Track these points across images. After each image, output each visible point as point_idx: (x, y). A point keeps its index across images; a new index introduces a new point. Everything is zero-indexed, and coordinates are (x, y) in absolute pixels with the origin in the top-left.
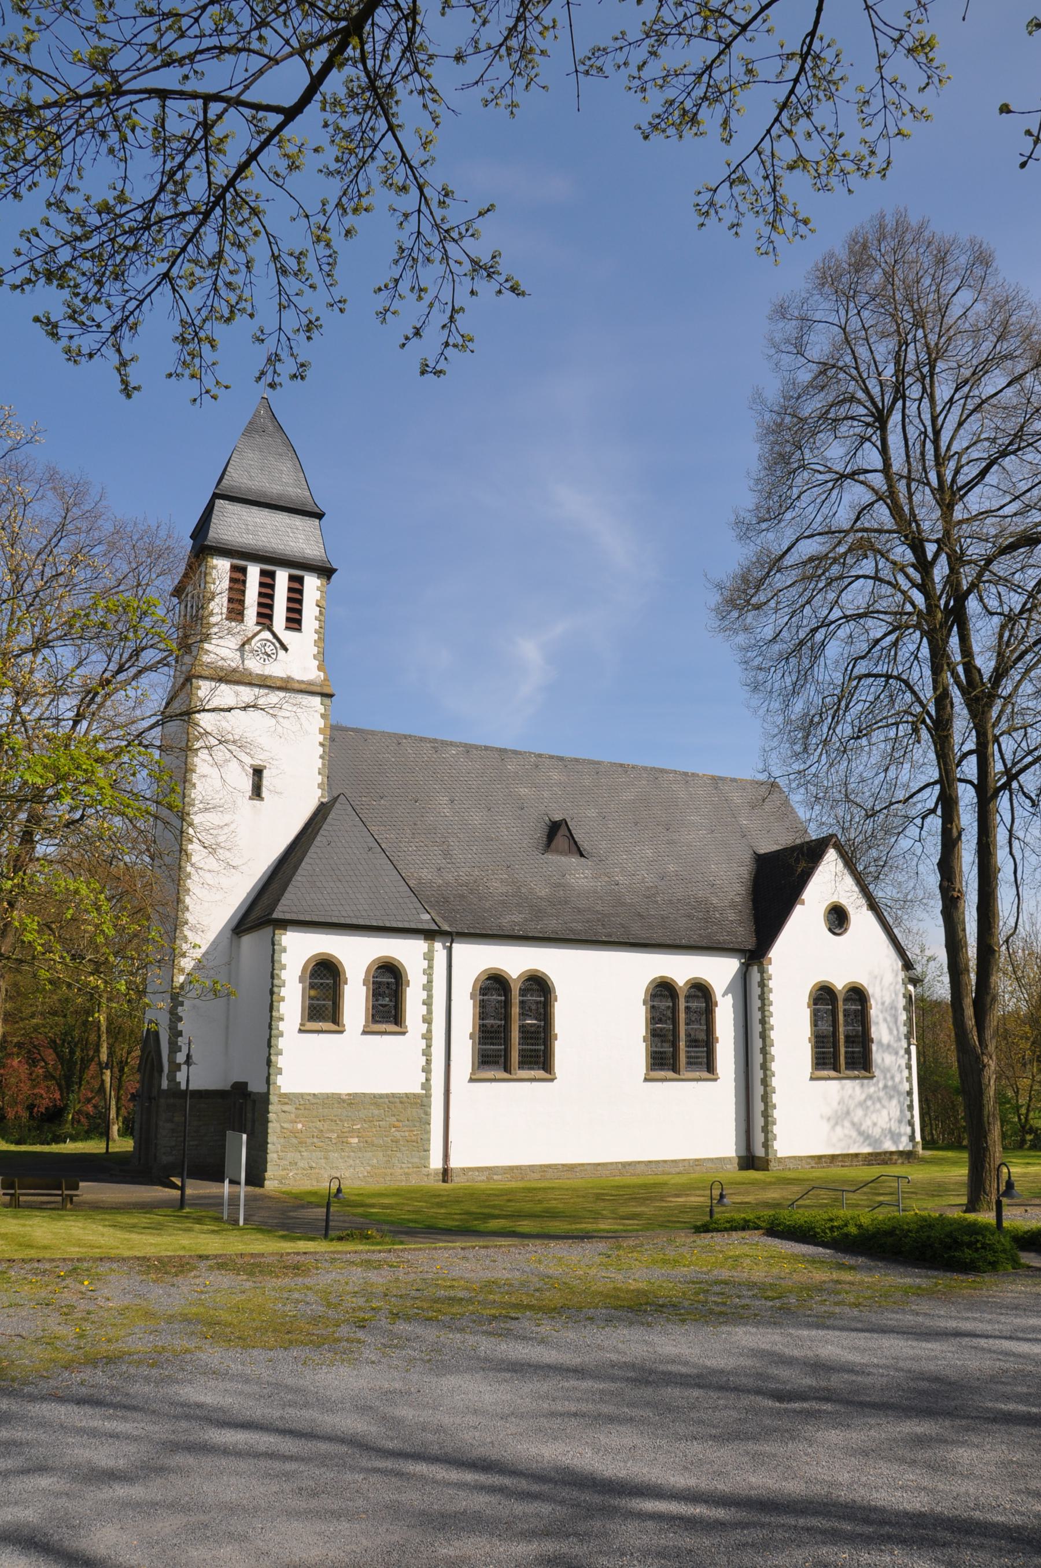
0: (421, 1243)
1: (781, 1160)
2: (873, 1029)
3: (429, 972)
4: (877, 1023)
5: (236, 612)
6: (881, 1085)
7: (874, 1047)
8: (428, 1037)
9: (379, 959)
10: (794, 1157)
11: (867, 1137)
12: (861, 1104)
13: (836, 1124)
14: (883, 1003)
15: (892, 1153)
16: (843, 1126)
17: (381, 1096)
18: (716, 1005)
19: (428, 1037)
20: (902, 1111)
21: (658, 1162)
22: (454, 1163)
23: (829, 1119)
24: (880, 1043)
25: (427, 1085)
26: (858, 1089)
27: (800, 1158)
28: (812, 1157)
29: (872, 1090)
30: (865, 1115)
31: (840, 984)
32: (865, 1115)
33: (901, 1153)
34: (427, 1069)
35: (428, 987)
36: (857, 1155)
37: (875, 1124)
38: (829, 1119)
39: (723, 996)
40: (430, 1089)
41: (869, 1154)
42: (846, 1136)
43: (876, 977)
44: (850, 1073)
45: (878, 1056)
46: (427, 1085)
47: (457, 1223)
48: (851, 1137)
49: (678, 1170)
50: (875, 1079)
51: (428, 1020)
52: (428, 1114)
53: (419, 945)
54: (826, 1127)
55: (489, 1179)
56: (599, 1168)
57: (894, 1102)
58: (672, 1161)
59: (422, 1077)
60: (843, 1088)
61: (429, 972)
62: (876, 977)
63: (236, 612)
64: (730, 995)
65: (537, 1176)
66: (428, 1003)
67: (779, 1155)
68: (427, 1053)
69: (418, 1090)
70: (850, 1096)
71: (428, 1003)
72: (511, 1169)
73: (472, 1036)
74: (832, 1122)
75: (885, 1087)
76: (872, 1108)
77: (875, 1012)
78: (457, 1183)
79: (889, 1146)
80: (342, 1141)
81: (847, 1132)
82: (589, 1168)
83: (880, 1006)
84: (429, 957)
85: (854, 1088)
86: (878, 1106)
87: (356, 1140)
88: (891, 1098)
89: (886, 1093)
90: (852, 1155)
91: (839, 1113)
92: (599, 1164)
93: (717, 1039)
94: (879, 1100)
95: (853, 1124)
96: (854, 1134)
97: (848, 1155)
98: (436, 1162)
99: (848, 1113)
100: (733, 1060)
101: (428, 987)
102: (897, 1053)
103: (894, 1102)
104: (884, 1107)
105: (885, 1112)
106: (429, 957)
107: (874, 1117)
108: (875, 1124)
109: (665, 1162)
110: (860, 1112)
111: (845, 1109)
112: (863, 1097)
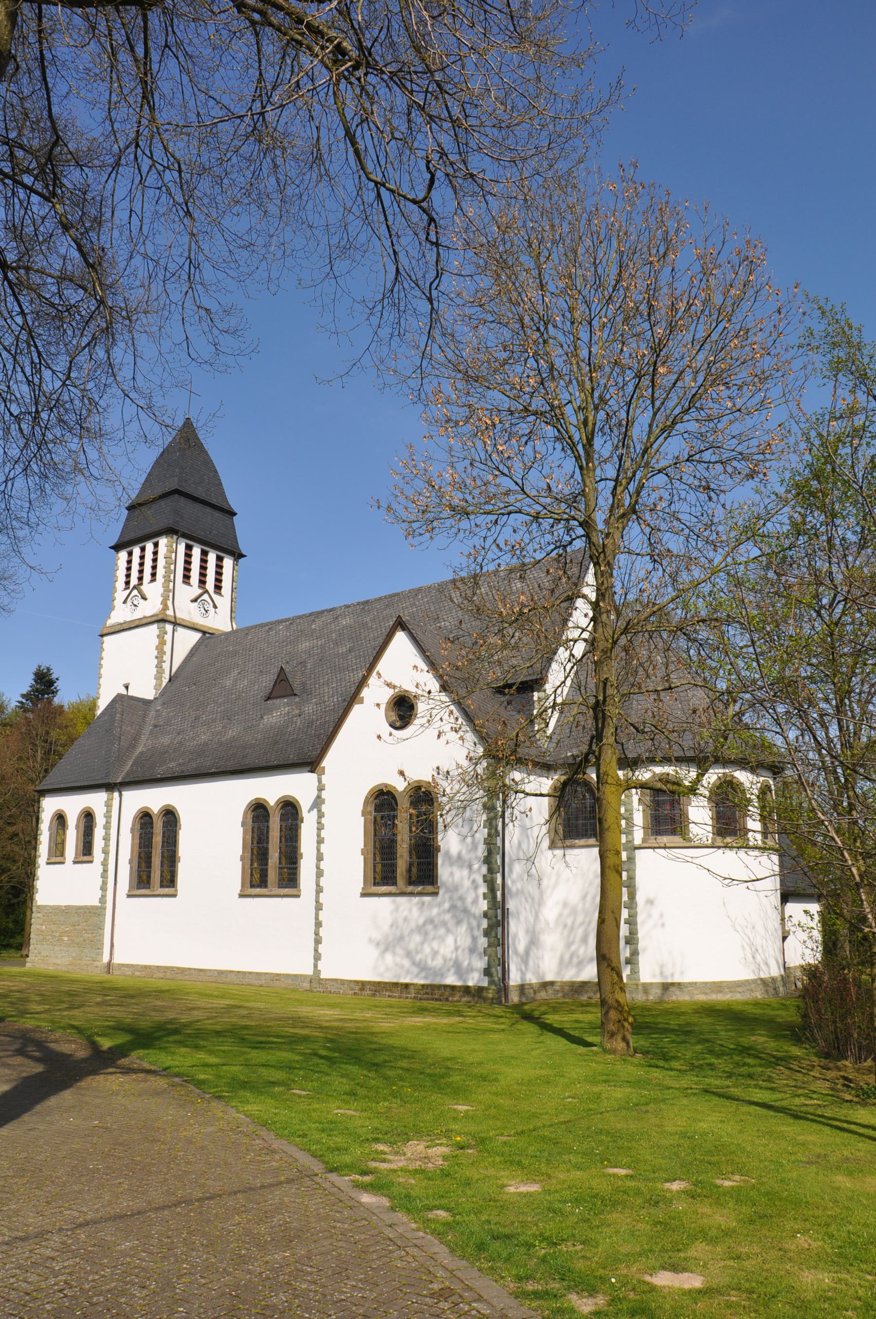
0: (282, 1031)
5: (187, 578)
6: (447, 905)
8: (105, 864)
9: (174, 807)
10: (336, 980)
11: (423, 967)
12: (420, 929)
13: (386, 949)
15: (453, 988)
16: (394, 953)
17: (80, 908)
18: (302, 821)
20: (474, 939)
21: (244, 973)
22: (117, 960)
23: (378, 944)
24: (447, 854)
25: (103, 899)
26: (415, 912)
27: (343, 982)
28: (357, 982)
29: (435, 911)
30: (422, 943)
33: (466, 990)
35: (107, 827)
36: (407, 986)
38: (378, 944)
39: (309, 812)
40: (105, 903)
41: (423, 986)
42: (396, 964)
44: (410, 889)
45: (444, 872)
46: (103, 899)
48: (402, 967)
49: (260, 983)
50: (439, 898)
51: (106, 852)
54: (374, 953)
56: (202, 973)
57: (463, 928)
58: (257, 973)
60: (397, 909)
63: (187, 578)
65: (160, 975)
66: (106, 838)
67: (322, 977)
71: (106, 838)
72: (146, 967)
74: (382, 947)
75: (453, 907)
79: (451, 980)
80: (60, 939)
81: (398, 960)
82: (193, 972)
85: (410, 910)
87: (66, 938)
88: (459, 922)
89: (454, 916)
90: (402, 984)
91: (390, 938)
92: (201, 970)
93: (301, 855)
94: (444, 924)
95: (408, 954)
96: (406, 963)
97: (396, 984)
98: (106, 959)
101: (107, 827)
102: (470, 867)
103: (463, 928)
104: (448, 931)
105: (450, 940)
106: (108, 805)
107: (435, 945)
108: (435, 953)
109: (250, 973)
110: (417, 938)
111: (398, 934)
112: (421, 921)
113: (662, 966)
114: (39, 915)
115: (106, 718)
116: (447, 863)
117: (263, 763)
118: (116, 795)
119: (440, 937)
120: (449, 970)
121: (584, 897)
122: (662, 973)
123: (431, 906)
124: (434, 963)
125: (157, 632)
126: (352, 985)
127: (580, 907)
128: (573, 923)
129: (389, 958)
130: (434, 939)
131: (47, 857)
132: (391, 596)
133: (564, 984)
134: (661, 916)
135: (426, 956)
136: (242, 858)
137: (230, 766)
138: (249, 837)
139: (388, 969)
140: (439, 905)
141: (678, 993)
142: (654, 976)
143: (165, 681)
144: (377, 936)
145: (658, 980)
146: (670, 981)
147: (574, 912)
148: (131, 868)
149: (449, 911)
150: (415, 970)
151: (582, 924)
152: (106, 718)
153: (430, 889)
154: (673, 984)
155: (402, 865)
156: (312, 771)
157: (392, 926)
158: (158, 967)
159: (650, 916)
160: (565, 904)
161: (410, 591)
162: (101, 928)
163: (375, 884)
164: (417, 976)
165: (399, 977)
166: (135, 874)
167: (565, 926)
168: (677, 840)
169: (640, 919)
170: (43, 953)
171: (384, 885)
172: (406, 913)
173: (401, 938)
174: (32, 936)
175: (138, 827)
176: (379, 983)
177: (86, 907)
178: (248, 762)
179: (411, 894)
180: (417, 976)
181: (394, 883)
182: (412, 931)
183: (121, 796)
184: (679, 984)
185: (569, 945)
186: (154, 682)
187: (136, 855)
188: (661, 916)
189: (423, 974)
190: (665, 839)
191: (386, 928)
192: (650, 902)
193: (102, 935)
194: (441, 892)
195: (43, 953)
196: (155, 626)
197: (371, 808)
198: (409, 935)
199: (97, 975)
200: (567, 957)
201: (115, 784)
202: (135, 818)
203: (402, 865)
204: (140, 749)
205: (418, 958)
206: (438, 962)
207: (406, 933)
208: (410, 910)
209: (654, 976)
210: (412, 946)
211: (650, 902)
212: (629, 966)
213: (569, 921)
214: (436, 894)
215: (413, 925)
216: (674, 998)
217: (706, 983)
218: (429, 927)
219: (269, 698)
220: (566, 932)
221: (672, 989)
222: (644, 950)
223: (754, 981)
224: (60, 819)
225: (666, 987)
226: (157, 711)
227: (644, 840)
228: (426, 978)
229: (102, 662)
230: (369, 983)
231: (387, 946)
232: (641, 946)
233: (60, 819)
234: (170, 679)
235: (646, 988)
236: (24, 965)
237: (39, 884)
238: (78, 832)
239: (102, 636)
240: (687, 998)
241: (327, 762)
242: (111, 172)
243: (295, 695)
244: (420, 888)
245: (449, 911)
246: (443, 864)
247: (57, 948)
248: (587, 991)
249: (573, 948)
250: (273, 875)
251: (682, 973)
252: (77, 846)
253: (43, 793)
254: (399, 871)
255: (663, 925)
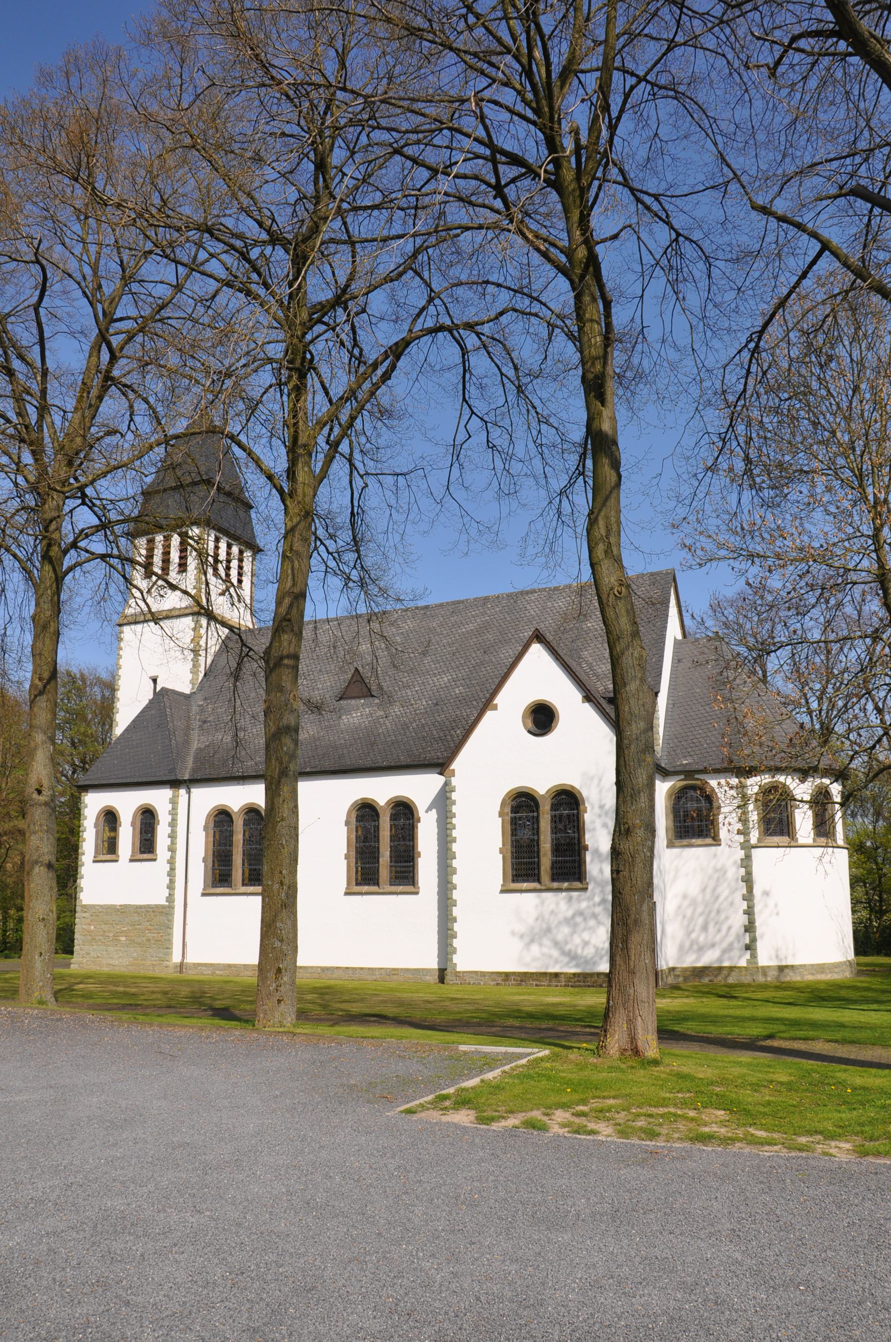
1: (457, 974)
2: (587, 836)
3: (174, 813)
4: (594, 829)
6: (597, 899)
7: (588, 857)
8: (172, 862)
11: (573, 957)
12: (568, 921)
13: (532, 941)
14: (602, 807)
16: (541, 945)
17: (141, 907)
19: (172, 862)
23: (522, 936)
25: (170, 898)
26: (563, 906)
27: (483, 974)
28: (499, 974)
29: (584, 905)
30: (572, 934)
31: (542, 786)
32: (572, 934)
34: (171, 886)
35: (173, 824)
36: (556, 975)
37: (586, 943)
38: (522, 936)
39: (427, 811)
41: (574, 974)
42: (544, 955)
43: (592, 778)
44: (555, 885)
46: (170, 898)
47: (673, 1051)
48: (550, 957)
49: (374, 977)
50: (588, 893)
51: (172, 849)
52: (171, 921)
53: (166, 793)
55: (213, 974)
59: (166, 892)
60: (543, 903)
61: (174, 813)
62: (592, 778)
64: (434, 811)
66: (173, 836)
67: (458, 969)
68: (172, 873)
69: (163, 902)
70: (552, 912)
71: (173, 836)
72: (229, 966)
73: (419, 855)
74: (527, 939)
76: (582, 925)
77: (588, 818)
78: (190, 975)
80: (116, 938)
81: (545, 950)
83: (597, 810)
84: (174, 802)
85: (557, 904)
86: (592, 923)
87: (123, 939)
90: (551, 974)
91: (536, 930)
93: (419, 854)
94: (594, 916)
95: (556, 944)
96: (555, 953)
97: (545, 974)
99: (548, 930)
100: (436, 874)
101: (173, 824)
106: (174, 802)
107: (586, 936)
109: (362, 969)
110: (566, 930)
111: (544, 926)
112: (570, 913)
113: (777, 951)
114: (85, 915)
115: (153, 712)
116: (596, 860)
117: (369, 764)
118: (182, 792)
119: (590, 928)
120: (601, 958)
121: (704, 890)
122: (777, 956)
123: (579, 901)
124: (585, 953)
125: (192, 625)
126: (493, 977)
127: (700, 898)
128: (693, 913)
129: (535, 949)
130: (584, 930)
131: (93, 854)
132: (453, 603)
133: (685, 970)
134: (776, 906)
135: (577, 946)
136: (347, 857)
137: (327, 765)
138: (353, 836)
139: (535, 959)
140: (589, 899)
141: (791, 974)
142: (771, 959)
143: (201, 675)
144: (521, 928)
145: (774, 963)
146: (784, 963)
147: (694, 903)
148: (206, 866)
149: (599, 904)
150: (566, 959)
151: (701, 914)
152: (153, 712)
153: (577, 884)
154: (787, 967)
155: (546, 861)
156: (441, 774)
157: (537, 919)
158: (245, 965)
159: (766, 906)
160: (685, 897)
161: (475, 599)
162: (169, 927)
163: (357, 884)
164: (567, 964)
165: (547, 967)
166: (210, 872)
167: (684, 917)
168: (785, 839)
169: (757, 909)
170: (93, 954)
171: (366, 884)
172: (552, 907)
173: (548, 930)
174: (76, 936)
175: (212, 825)
176: (525, 973)
177: (149, 906)
178: (348, 762)
179: (559, 890)
180: (567, 964)
181: (377, 884)
182: (560, 923)
183: (189, 793)
184: (792, 966)
185: (689, 934)
186: (190, 676)
187: (211, 853)
188: (776, 906)
189: (574, 963)
190: (776, 839)
191: (531, 920)
192: (766, 894)
193: (170, 935)
194: (590, 887)
195: (93, 954)
196: (190, 618)
197: (508, 809)
198: (557, 926)
199: (171, 974)
200: (687, 944)
201: (185, 781)
202: (209, 816)
203: (546, 861)
204: (195, 746)
205: (568, 947)
206: (589, 952)
207: (553, 925)
208: (557, 904)
209: (771, 959)
210: (560, 937)
211: (766, 894)
212: (749, 952)
213: (689, 913)
214: (586, 889)
215: (560, 917)
216: (788, 979)
217: (813, 965)
218: (579, 919)
219: (341, 699)
220: (685, 922)
221: (786, 971)
222: (762, 936)
223: (844, 963)
224: (110, 817)
225: (781, 969)
226: (199, 706)
227: (759, 840)
228: (577, 966)
229: (121, 652)
230: (514, 973)
231: (532, 938)
232: (758, 934)
233: (110, 817)
234: (205, 675)
235: (765, 970)
236: (68, 965)
237: (83, 883)
238: (134, 829)
239: (120, 625)
240: (799, 978)
241: (455, 765)
242: (427, 195)
243: (372, 696)
244: (566, 885)
245: (599, 904)
246: (592, 860)
247: (111, 949)
248: (708, 975)
249: (694, 936)
250: (384, 872)
251: (794, 955)
252: (133, 844)
253: (86, 788)
254: (542, 868)
255: (778, 914)
